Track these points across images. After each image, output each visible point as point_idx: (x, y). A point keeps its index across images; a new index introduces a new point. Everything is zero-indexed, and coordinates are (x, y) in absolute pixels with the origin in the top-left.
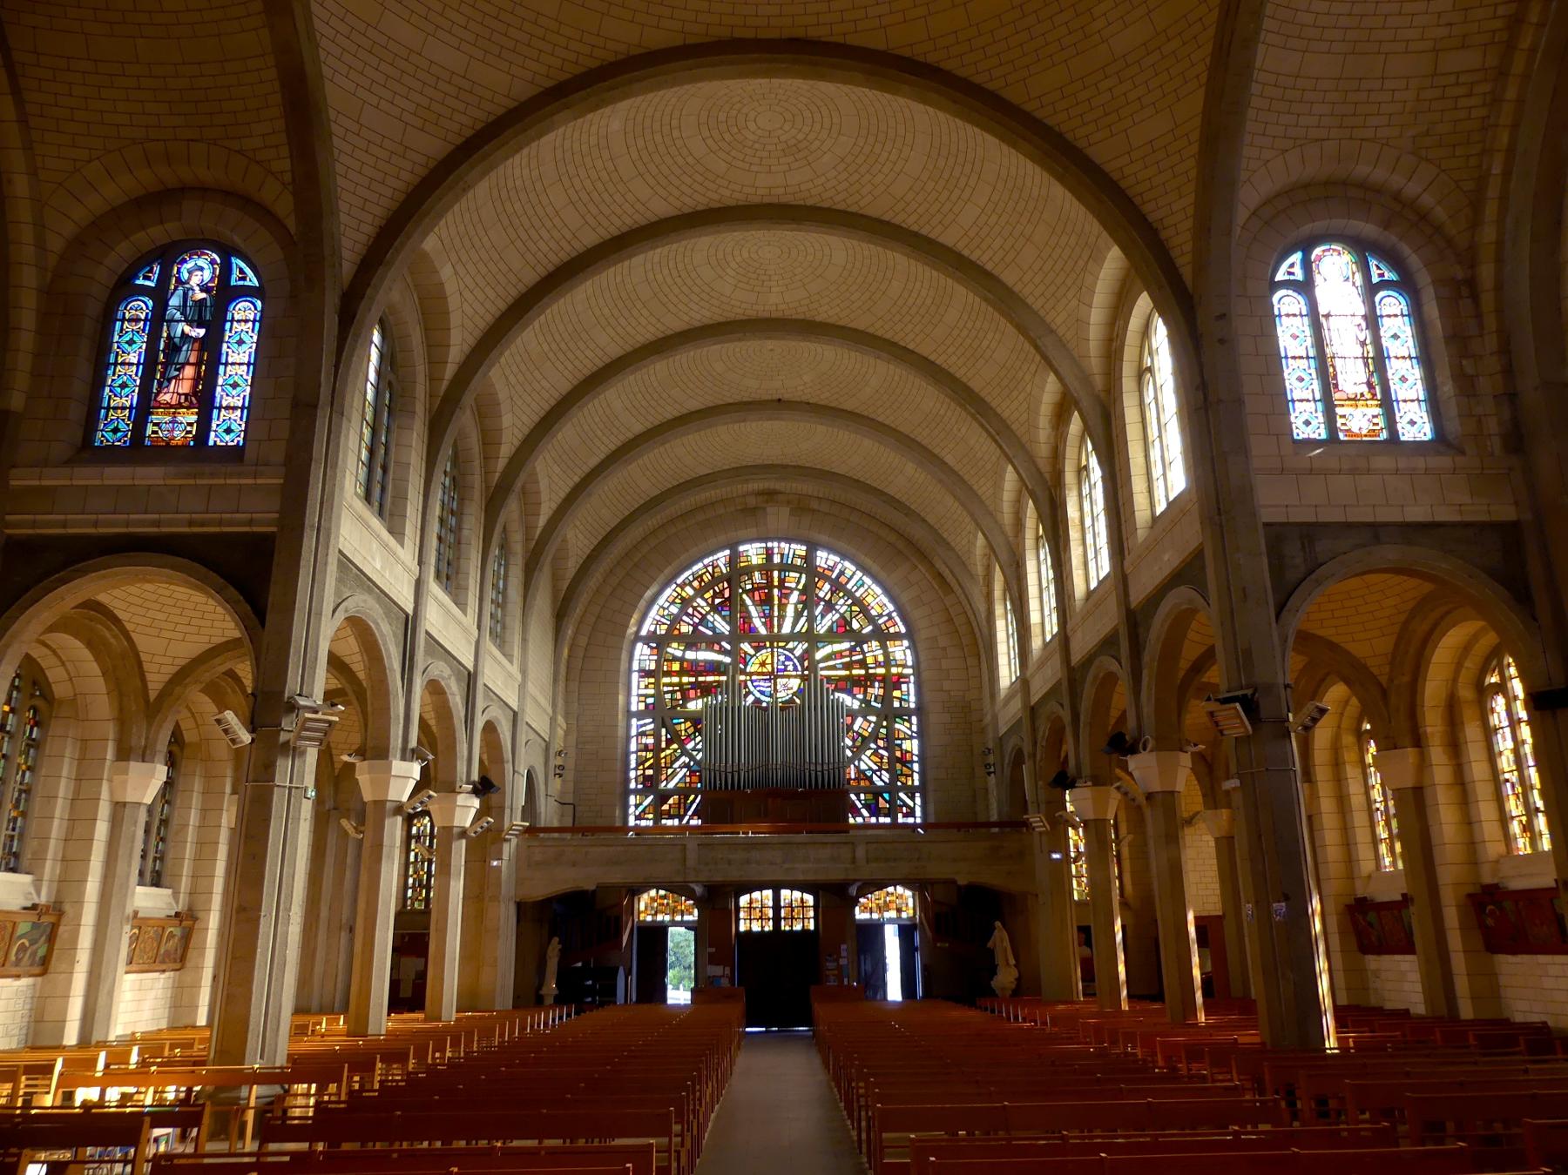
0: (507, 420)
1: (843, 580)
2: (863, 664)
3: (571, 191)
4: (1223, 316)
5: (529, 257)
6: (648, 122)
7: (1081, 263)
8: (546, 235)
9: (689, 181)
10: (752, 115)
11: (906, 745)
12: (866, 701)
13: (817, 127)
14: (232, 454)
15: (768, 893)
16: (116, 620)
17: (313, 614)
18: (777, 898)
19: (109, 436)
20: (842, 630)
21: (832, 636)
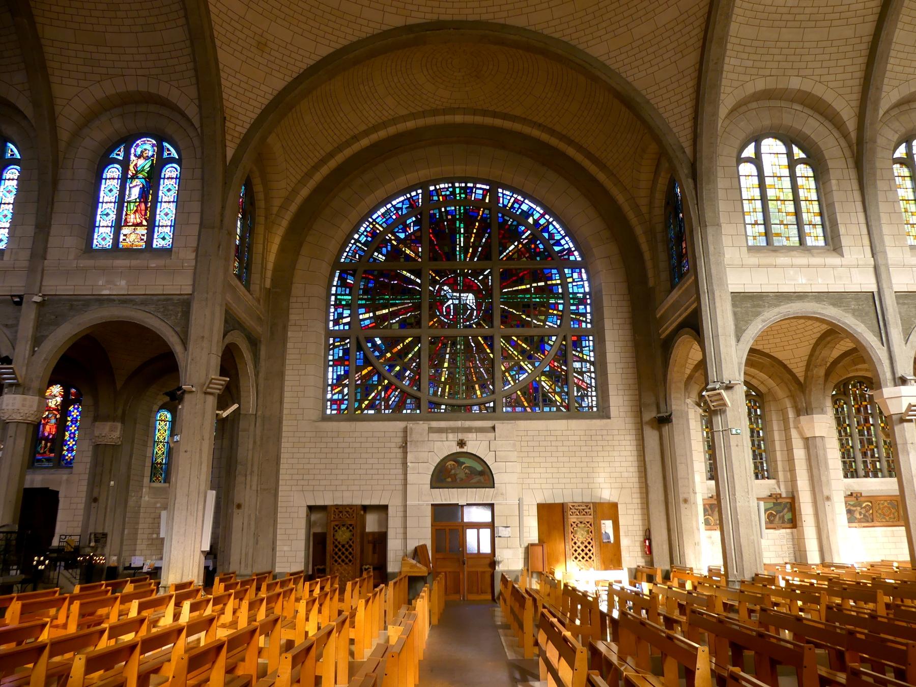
14: (163, 251)
15: (793, 210)
19: (161, 241)
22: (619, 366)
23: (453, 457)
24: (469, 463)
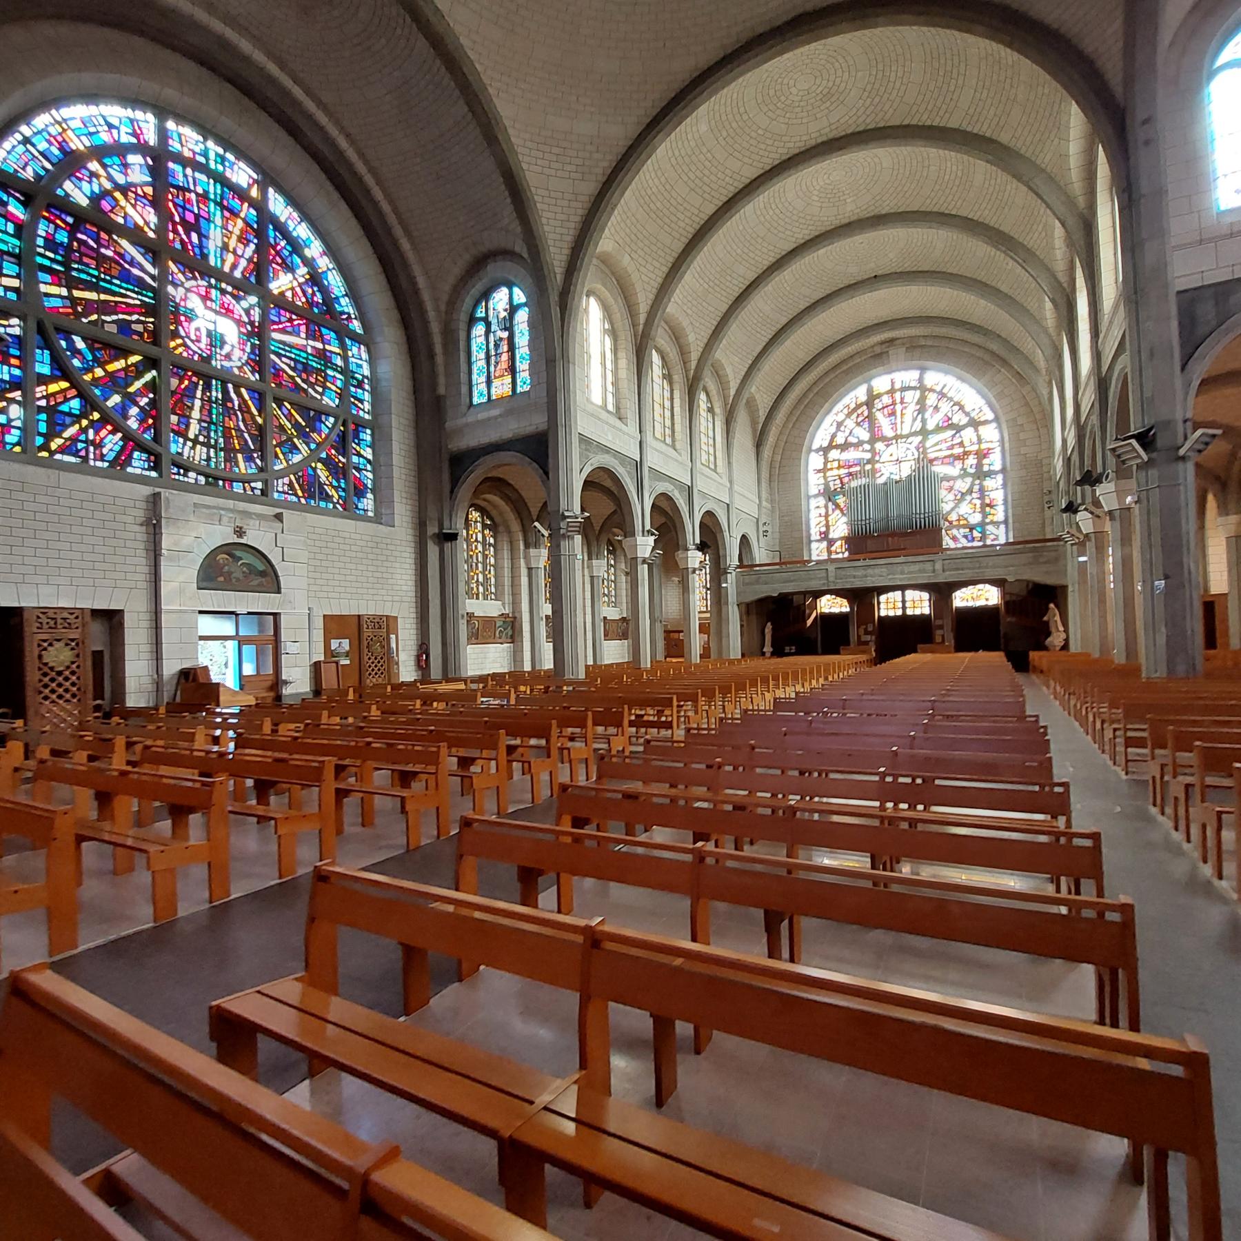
0: (691, 338)
1: (945, 391)
2: (961, 444)
3: (690, 183)
4: (1146, 121)
5: (674, 233)
6: (724, 118)
7: (1056, 106)
8: (682, 217)
9: (763, 146)
10: (792, 82)
11: (993, 495)
12: (963, 469)
13: (839, 73)
15: (899, 593)
16: (509, 485)
17: (569, 470)
18: (903, 596)
20: (949, 425)
21: (938, 429)
22: (403, 471)
23: (227, 549)
24: (247, 558)
